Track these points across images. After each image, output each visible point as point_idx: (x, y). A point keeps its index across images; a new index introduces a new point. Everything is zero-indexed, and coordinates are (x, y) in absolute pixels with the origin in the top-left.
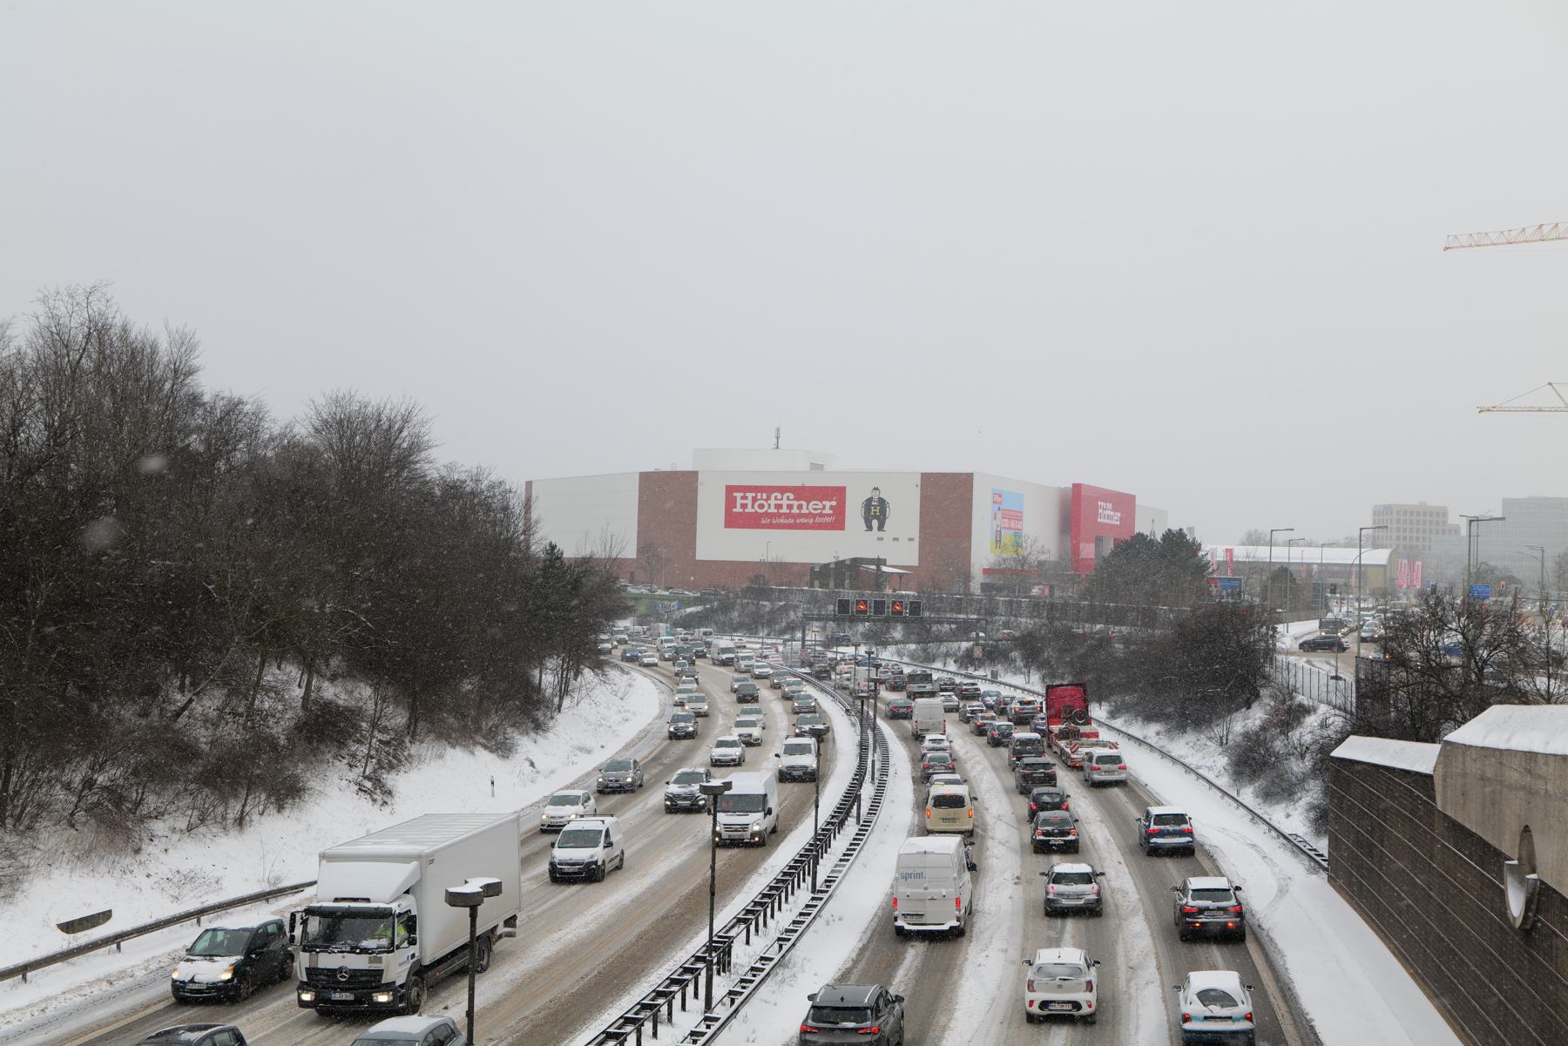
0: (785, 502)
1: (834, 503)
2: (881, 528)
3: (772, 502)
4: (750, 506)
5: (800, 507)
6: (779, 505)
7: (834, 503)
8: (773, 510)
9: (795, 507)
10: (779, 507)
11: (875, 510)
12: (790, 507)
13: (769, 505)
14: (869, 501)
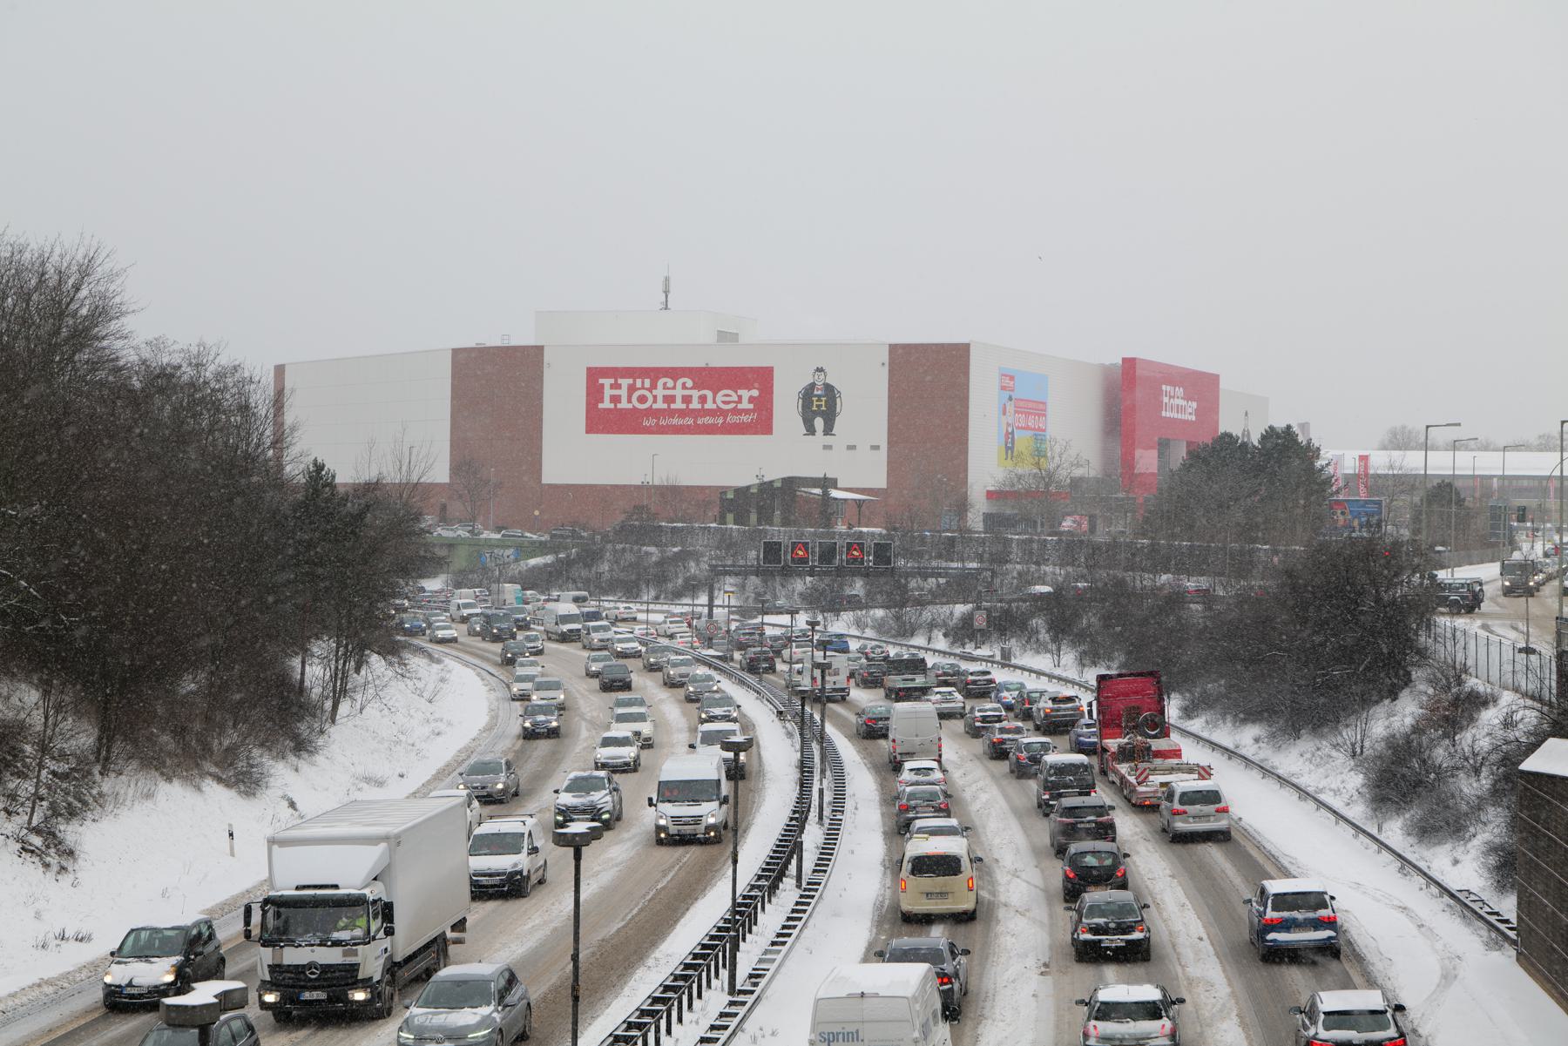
0: (679, 393)
1: (755, 393)
5: (703, 399)
7: (755, 393)
8: (660, 405)
10: (669, 399)
11: (819, 404)
12: (687, 399)
14: (812, 386)
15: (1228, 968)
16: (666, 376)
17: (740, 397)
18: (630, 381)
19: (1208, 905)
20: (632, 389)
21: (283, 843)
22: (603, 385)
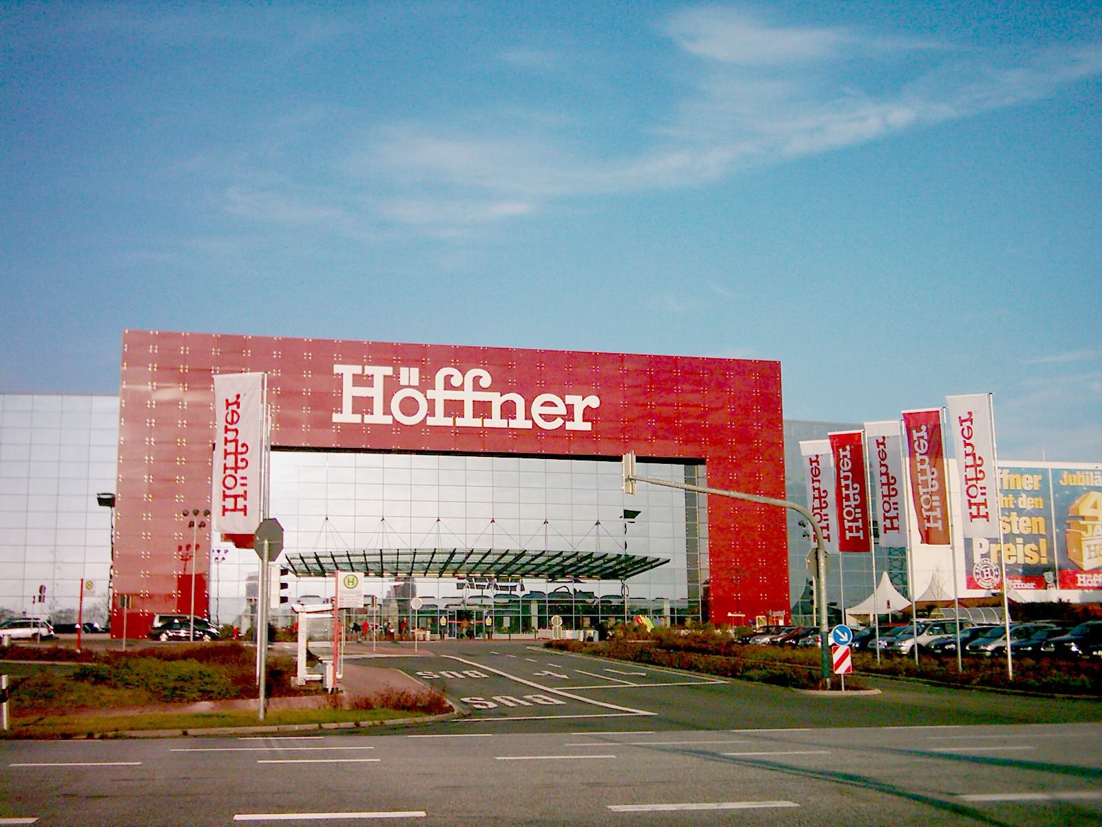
0: (469, 397)
1: (594, 402)
3: (439, 394)
4: (378, 405)
5: (508, 410)
9: (496, 411)
10: (454, 408)
13: (431, 403)
16: (940, 486)
17: (570, 408)
18: (389, 371)
20: (392, 385)
21: (373, 598)
22: (850, 537)
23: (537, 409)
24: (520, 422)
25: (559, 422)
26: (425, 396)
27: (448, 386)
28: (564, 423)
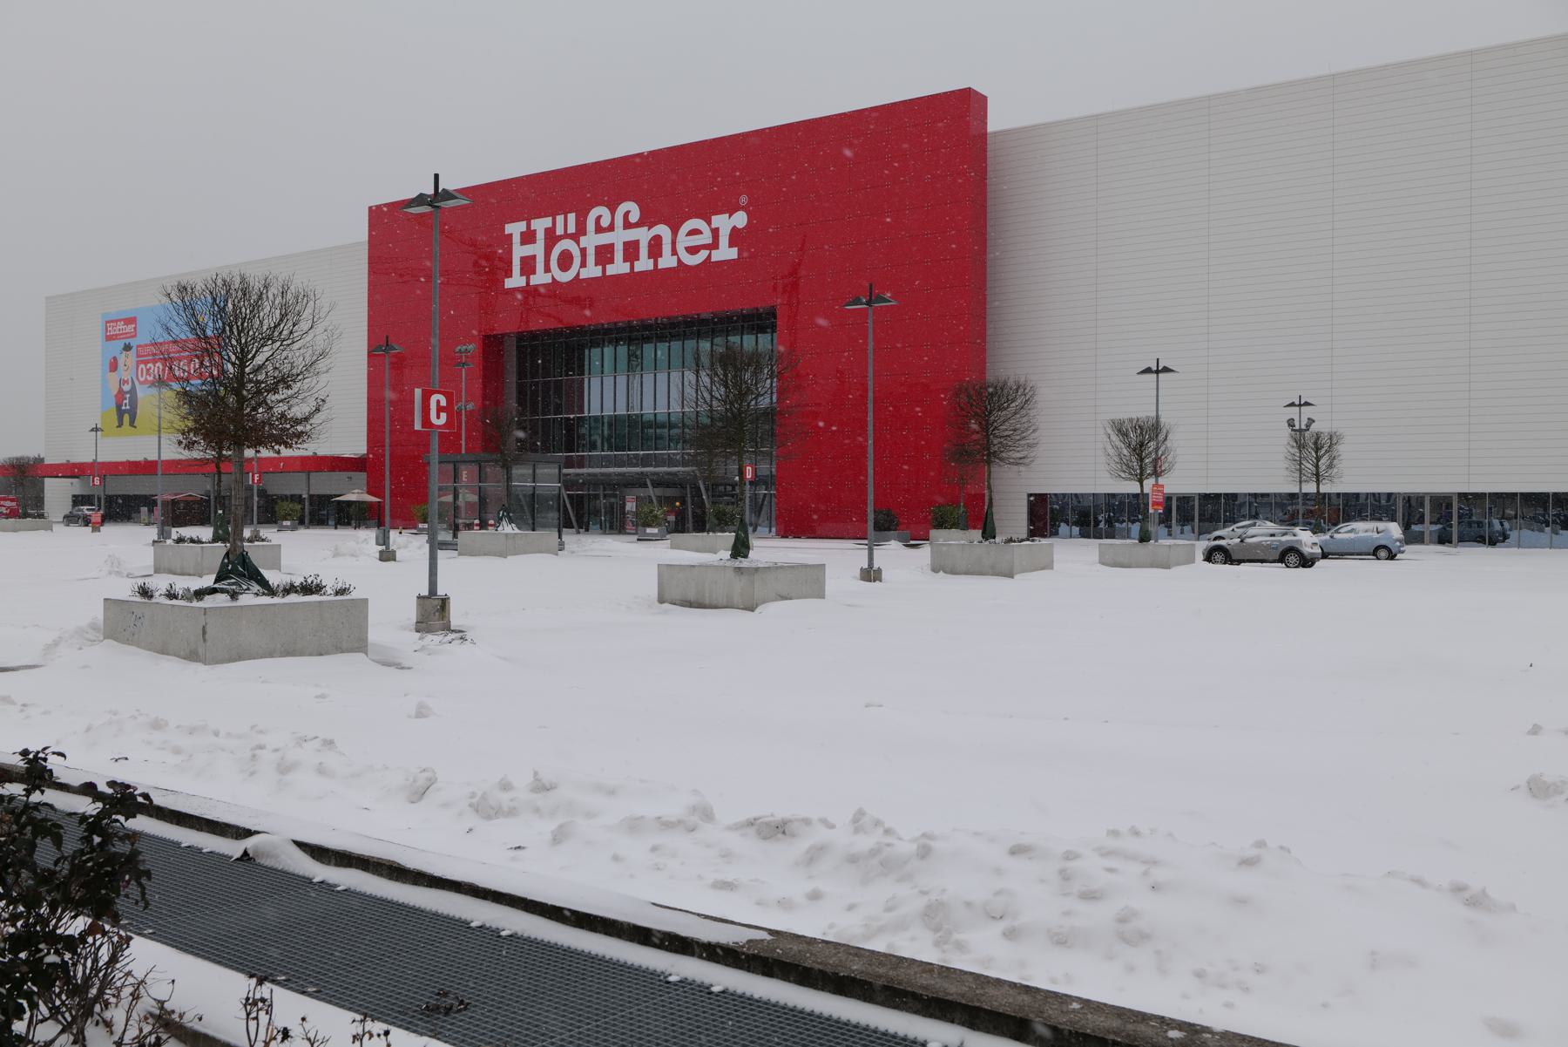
0: (619, 237)
1: (740, 220)
2: (132, 423)
3: (591, 241)
5: (655, 248)
6: (625, 250)
7: (740, 220)
13: (583, 251)
15: (1115, 1023)
17: (715, 233)
19: (1198, 1025)
23: (684, 241)
24: (667, 261)
25: (703, 254)
26: (579, 245)
27: (599, 229)
28: (710, 254)
